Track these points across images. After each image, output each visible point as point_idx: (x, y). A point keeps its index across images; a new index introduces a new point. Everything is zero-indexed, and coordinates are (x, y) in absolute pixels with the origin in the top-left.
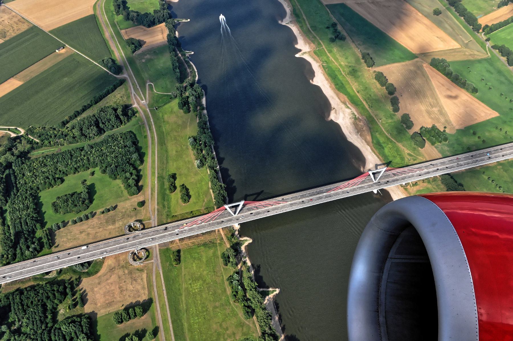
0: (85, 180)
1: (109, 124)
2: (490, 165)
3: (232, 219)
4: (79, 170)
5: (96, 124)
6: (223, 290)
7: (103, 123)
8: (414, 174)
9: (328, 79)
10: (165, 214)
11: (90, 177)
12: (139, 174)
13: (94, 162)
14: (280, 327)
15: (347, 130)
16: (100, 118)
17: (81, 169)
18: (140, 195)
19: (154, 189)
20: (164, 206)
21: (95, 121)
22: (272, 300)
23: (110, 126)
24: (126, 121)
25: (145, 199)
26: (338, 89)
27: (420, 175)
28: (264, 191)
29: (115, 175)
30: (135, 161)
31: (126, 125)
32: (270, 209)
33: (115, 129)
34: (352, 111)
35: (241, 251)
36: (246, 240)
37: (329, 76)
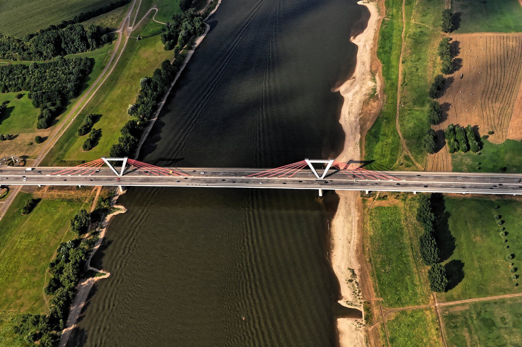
0: (8, 102)
1: (73, 45)
2: (518, 199)
3: (114, 179)
4: (9, 89)
5: (56, 42)
6: (49, 255)
7: (66, 43)
8: (383, 182)
9: (376, 39)
10: (56, 157)
11: (16, 99)
12: (64, 107)
13: (28, 84)
14: (78, 316)
15: (349, 108)
16: (63, 36)
17: (11, 89)
18: (48, 130)
19: (65, 126)
20: (61, 148)
21: (55, 38)
22: (93, 283)
23: (73, 49)
24: (95, 46)
25: (49, 135)
26: (379, 54)
27: (464, 188)
28: (375, 161)
29: (38, 102)
30: (68, 92)
31: (94, 51)
32: (68, 177)
33: (80, 52)
34: (375, 86)
35: (104, 219)
36: (118, 209)
37: (382, 35)
